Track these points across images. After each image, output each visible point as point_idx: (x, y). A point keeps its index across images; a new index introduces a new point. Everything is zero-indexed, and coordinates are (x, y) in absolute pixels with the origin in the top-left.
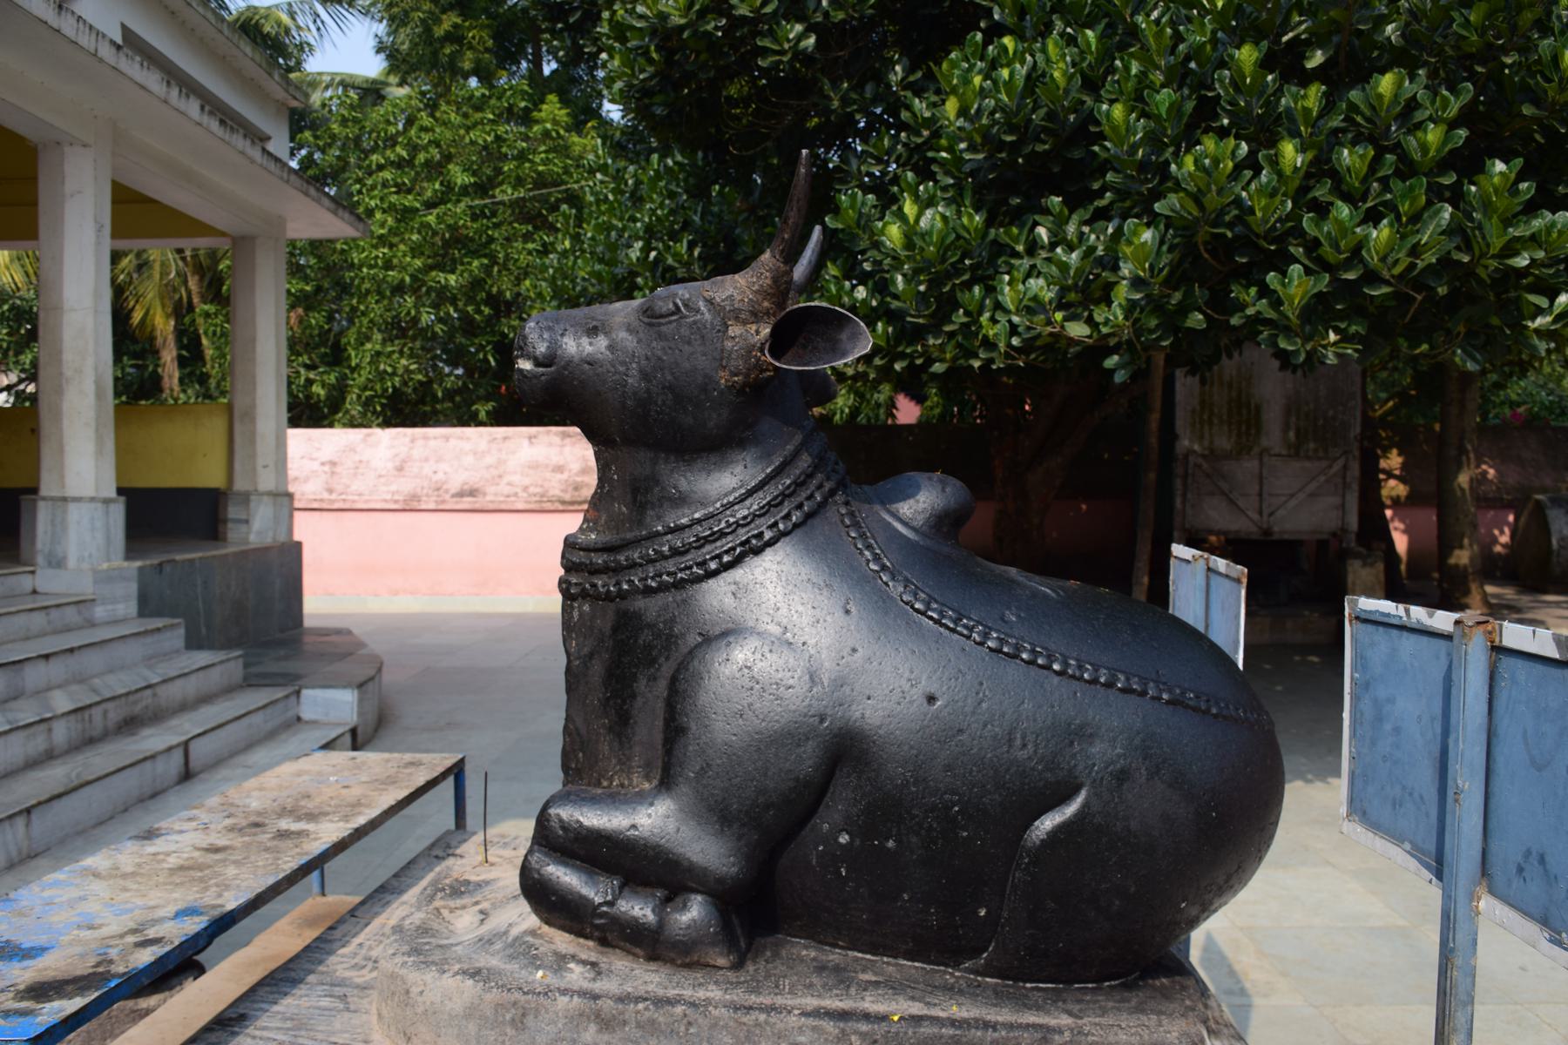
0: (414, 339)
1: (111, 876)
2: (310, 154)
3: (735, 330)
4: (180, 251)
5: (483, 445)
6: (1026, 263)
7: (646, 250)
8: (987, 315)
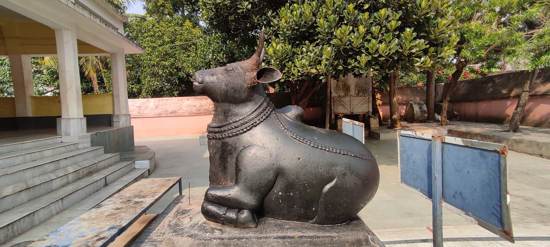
0: (158, 77)
1: (88, 220)
2: (128, 34)
3: (248, 74)
4: (96, 57)
5: (176, 101)
6: (301, 56)
7: (213, 55)
8: (293, 68)
